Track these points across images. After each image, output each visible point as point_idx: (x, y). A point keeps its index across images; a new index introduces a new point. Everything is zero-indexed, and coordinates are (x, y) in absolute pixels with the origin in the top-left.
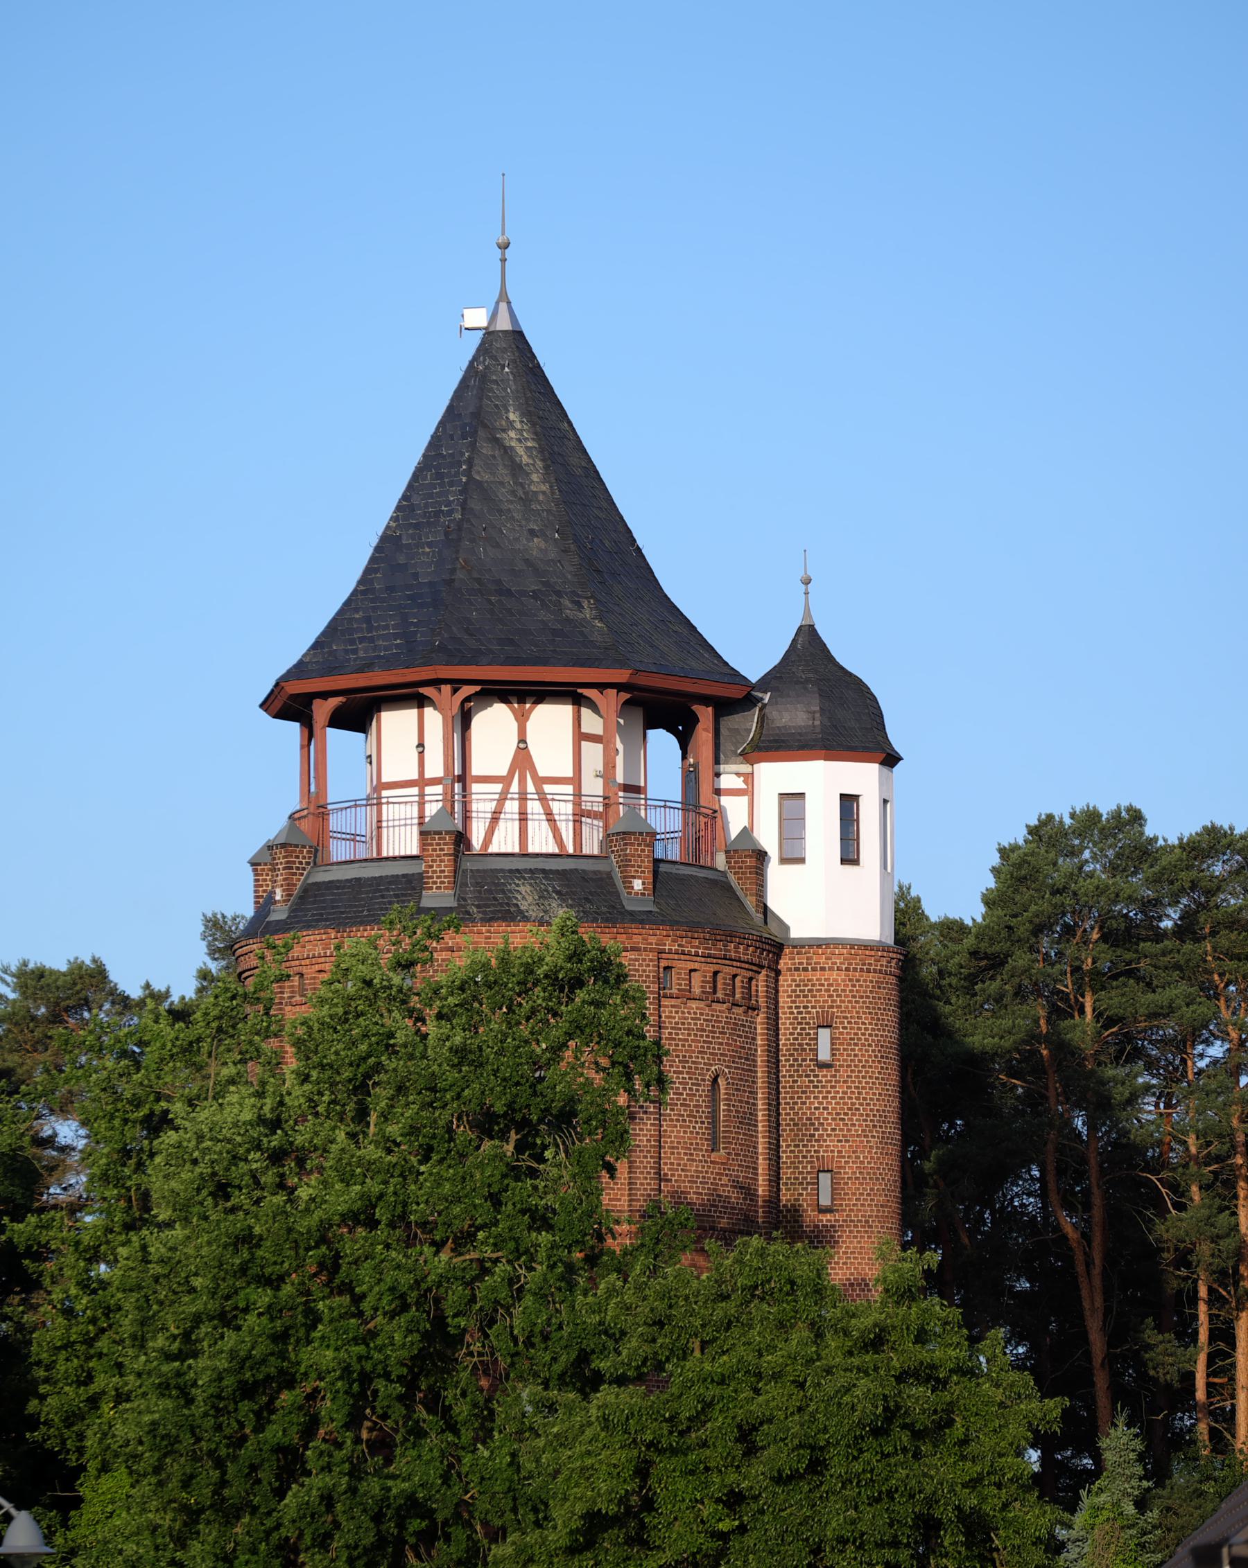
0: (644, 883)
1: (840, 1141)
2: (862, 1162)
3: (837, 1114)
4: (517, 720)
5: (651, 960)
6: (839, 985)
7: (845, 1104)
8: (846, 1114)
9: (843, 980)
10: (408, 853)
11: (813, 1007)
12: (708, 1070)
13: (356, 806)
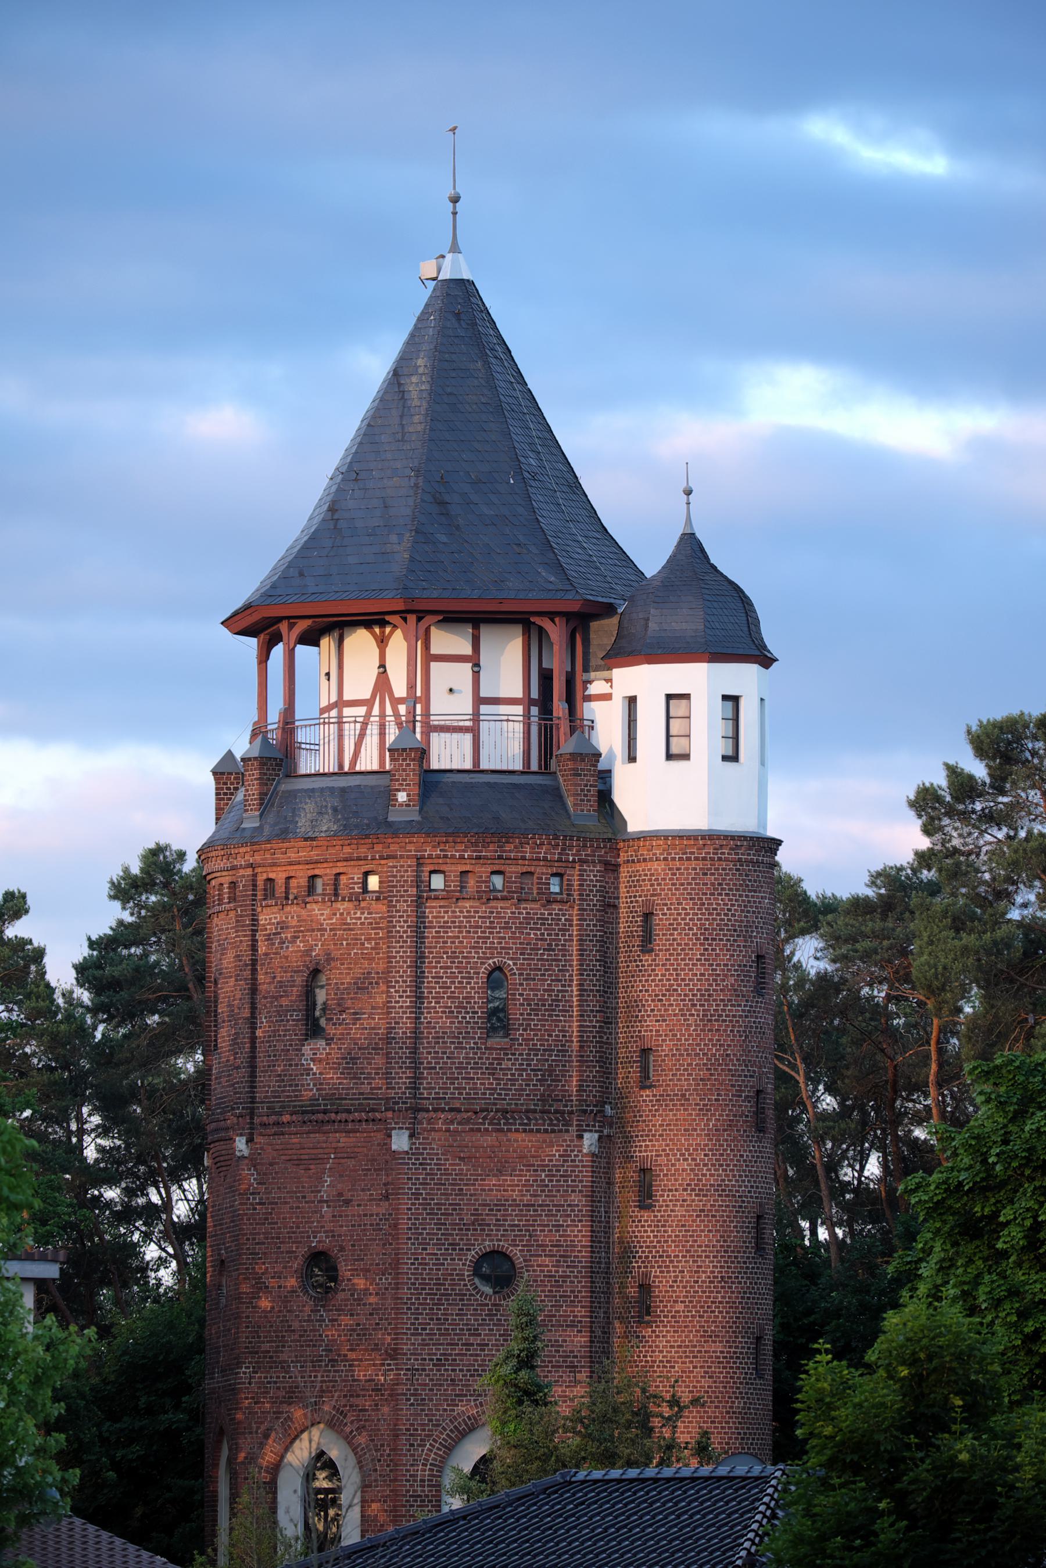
0: (408, 795)
1: (658, 1021)
2: (679, 1040)
3: (656, 995)
4: (378, 647)
5: (410, 866)
6: (659, 874)
7: (663, 985)
8: (664, 995)
9: (664, 870)
10: (369, 768)
11: (640, 896)
12: (483, 963)
13: (508, 720)
